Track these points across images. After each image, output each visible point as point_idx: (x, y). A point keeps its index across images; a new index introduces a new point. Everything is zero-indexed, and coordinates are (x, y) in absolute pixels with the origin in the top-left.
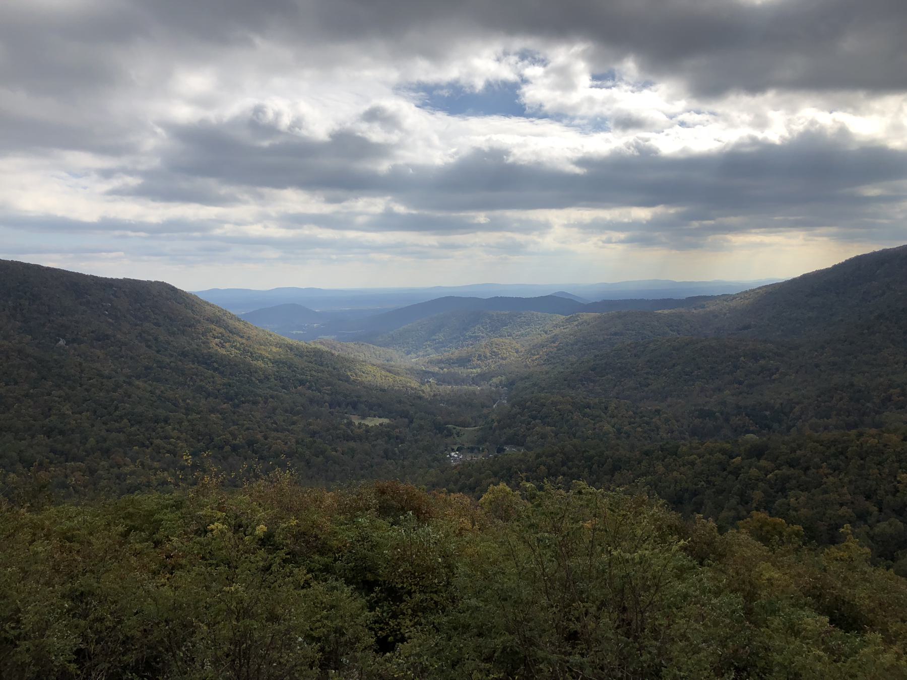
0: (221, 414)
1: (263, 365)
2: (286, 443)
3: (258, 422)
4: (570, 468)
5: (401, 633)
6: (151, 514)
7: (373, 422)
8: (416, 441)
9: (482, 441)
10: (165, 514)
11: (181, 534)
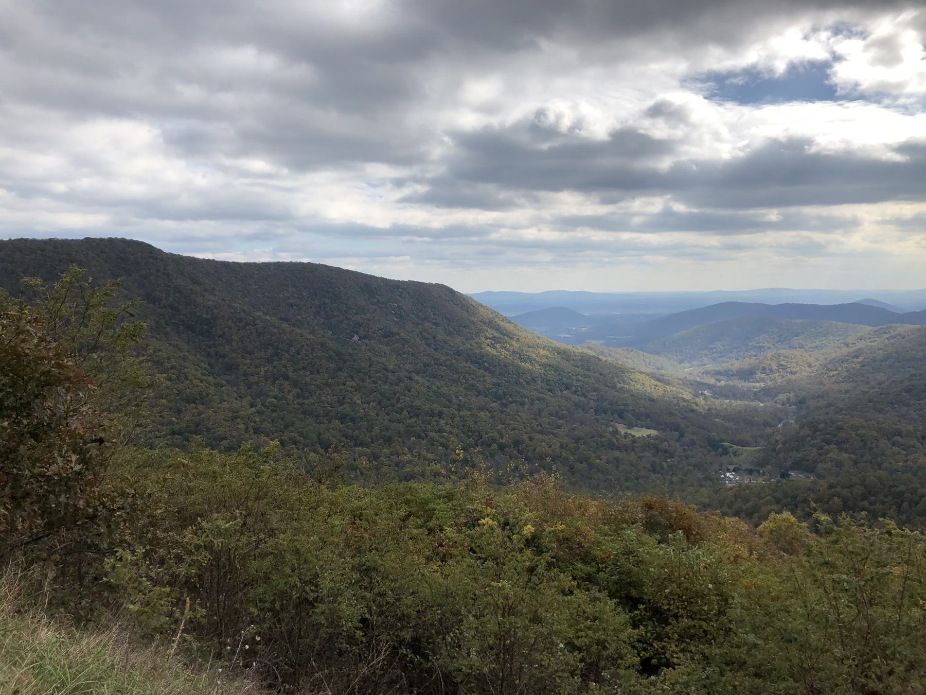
0: (489, 412)
1: (530, 367)
2: (550, 447)
3: (524, 423)
4: (871, 504)
5: (666, 657)
6: (426, 502)
7: (640, 433)
8: (687, 457)
9: (762, 463)
10: (438, 504)
11: (452, 524)
